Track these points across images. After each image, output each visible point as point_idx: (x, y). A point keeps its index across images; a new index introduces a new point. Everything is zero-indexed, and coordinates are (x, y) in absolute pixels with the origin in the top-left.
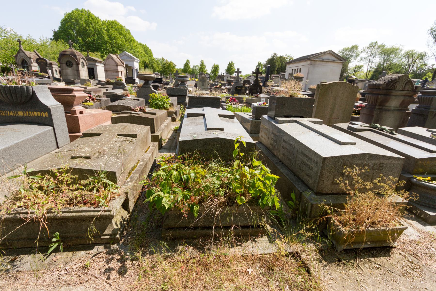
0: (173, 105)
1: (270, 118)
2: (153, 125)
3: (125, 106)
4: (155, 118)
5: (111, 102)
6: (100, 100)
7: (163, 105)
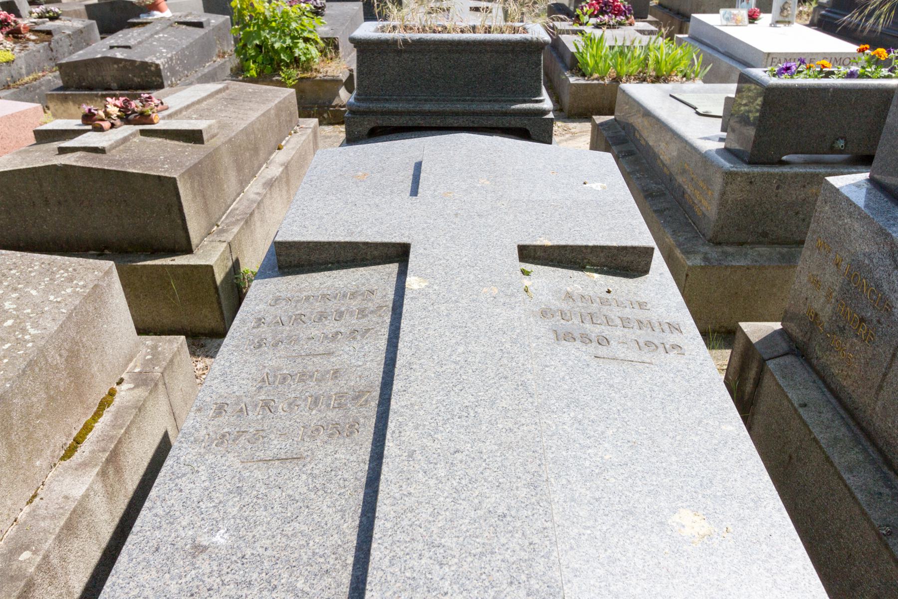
0: (336, 47)
1: (880, 195)
2: (175, 209)
3: (133, 62)
4: (194, 172)
5: (101, 33)
6: (49, 33)
7: (289, 49)
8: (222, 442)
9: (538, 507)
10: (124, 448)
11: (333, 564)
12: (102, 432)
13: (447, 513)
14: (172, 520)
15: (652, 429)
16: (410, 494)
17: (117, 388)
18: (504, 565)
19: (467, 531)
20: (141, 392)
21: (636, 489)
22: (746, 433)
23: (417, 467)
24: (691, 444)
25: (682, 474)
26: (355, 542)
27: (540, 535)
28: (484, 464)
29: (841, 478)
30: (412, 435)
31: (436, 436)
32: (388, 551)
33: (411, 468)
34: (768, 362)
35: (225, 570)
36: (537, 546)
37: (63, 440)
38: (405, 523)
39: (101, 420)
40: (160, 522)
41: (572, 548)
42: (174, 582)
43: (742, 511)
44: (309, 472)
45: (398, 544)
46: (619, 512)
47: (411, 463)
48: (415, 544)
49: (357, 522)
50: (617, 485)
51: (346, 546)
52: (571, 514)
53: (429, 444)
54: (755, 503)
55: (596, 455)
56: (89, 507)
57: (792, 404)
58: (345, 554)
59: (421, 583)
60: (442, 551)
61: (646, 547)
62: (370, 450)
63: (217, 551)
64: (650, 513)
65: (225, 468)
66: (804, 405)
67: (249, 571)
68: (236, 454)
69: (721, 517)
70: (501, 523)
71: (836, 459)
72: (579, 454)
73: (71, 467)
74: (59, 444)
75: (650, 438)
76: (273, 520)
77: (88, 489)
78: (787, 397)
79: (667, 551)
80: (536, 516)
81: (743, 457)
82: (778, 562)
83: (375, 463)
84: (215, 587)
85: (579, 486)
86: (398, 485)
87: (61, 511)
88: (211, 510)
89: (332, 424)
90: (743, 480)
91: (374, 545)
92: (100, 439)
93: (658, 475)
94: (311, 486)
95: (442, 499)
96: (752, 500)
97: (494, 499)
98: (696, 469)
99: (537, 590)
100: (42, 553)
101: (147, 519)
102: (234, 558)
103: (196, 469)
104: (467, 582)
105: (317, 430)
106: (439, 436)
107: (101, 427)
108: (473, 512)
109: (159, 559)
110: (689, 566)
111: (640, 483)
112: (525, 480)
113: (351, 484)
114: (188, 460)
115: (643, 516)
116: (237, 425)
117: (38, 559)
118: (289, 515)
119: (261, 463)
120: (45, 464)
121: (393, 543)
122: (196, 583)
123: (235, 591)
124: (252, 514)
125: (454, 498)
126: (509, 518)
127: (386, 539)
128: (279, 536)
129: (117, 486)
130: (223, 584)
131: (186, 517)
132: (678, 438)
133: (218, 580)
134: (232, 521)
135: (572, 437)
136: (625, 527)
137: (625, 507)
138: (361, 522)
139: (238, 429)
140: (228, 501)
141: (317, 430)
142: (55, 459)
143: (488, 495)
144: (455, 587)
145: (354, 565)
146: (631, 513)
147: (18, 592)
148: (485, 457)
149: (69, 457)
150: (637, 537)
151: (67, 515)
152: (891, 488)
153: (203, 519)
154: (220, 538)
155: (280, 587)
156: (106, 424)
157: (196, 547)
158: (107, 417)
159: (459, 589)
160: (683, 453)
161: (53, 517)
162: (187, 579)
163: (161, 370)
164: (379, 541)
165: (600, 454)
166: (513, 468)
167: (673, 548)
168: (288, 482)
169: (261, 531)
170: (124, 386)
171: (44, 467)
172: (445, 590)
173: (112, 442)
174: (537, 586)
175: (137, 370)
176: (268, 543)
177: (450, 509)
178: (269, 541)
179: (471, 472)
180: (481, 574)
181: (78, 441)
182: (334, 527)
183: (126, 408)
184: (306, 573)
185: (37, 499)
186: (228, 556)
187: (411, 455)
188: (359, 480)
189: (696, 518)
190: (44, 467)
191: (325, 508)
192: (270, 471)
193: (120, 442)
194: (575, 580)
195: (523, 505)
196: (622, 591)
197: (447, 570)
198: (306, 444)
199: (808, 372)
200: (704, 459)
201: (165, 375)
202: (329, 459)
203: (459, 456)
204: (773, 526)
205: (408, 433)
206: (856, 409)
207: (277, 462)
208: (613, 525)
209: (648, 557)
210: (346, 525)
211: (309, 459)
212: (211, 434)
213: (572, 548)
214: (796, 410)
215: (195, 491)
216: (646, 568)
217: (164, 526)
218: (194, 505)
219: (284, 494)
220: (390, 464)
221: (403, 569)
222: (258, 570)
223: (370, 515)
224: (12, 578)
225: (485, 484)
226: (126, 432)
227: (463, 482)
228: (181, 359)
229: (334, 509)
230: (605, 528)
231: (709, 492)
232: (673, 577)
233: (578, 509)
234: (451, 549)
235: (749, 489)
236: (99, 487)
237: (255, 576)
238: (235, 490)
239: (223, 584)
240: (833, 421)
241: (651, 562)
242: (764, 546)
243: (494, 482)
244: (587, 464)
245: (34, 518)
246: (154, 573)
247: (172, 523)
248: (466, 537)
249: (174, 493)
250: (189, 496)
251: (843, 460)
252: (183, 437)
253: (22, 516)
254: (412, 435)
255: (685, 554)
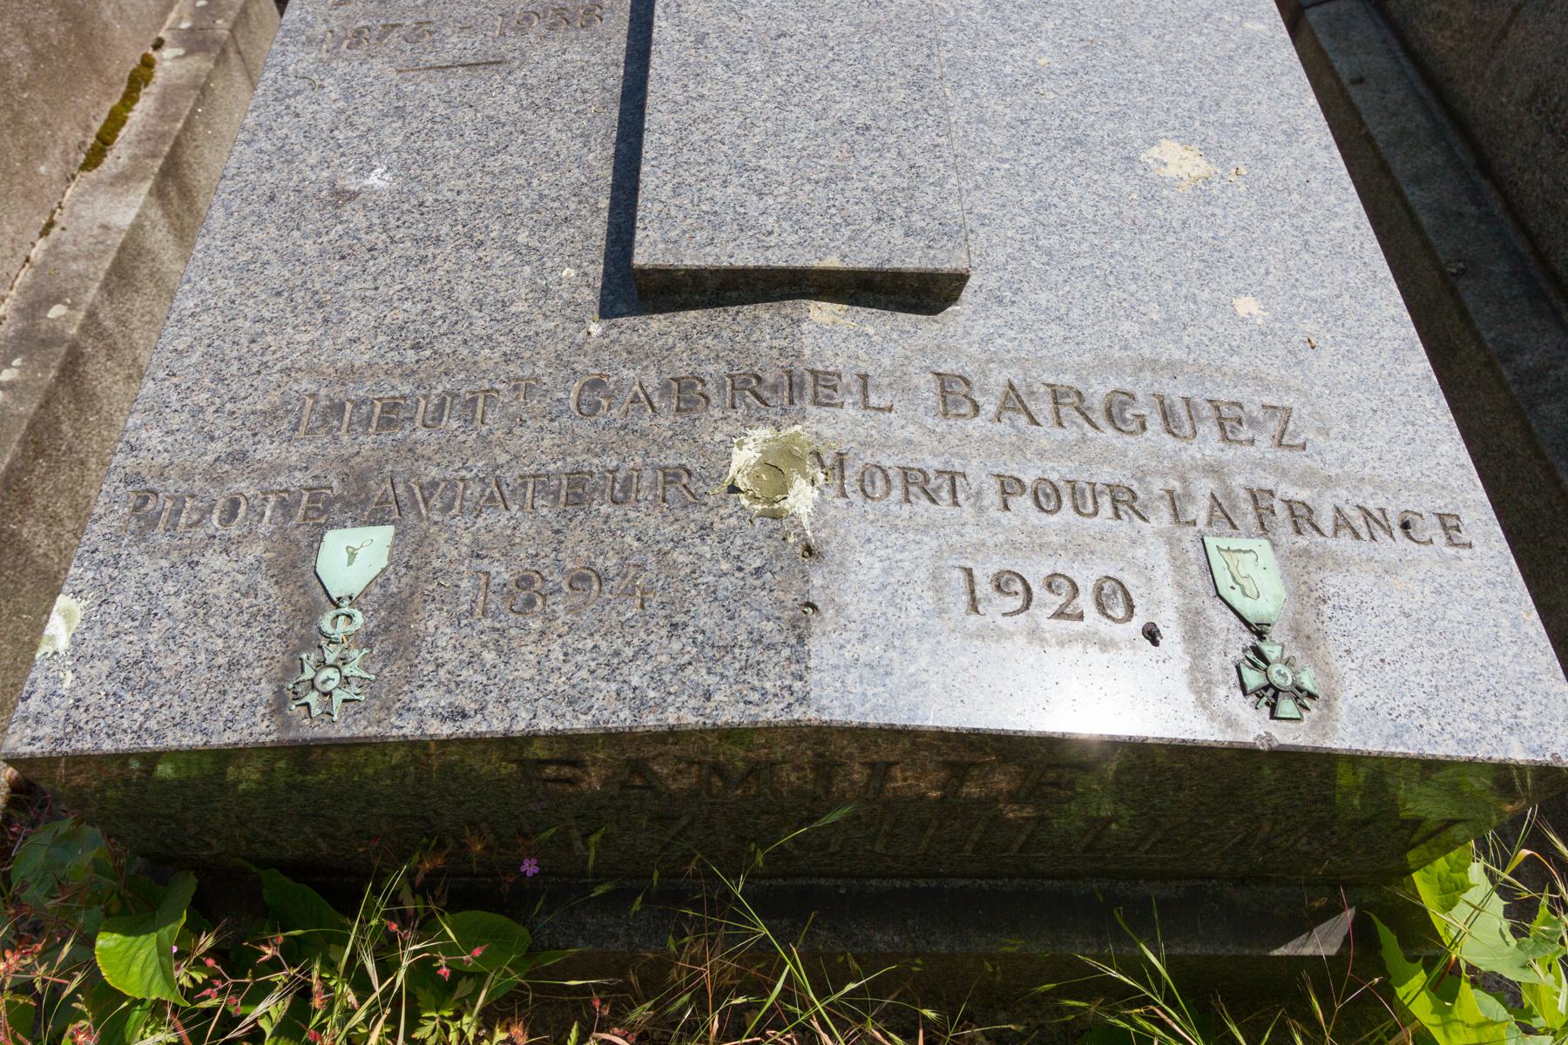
8: (359, 43)
9: (926, 116)
10: (188, 155)
11: (576, 210)
12: (144, 127)
13: (769, 124)
14: (289, 158)
15: (1124, 22)
16: (702, 96)
17: (155, 55)
18: (865, 195)
19: (804, 149)
20: (200, 64)
21: (1090, 109)
22: (1286, 35)
23: (712, 57)
24: (1189, 48)
25: (1170, 91)
26: (610, 178)
27: (928, 155)
28: (830, 54)
29: (1399, 194)
30: (700, 10)
31: (743, 12)
32: (669, 177)
33: (702, 59)
34: (1308, 12)
35: (393, 223)
36: (922, 170)
37: (75, 135)
38: (696, 137)
39: (138, 107)
40: (269, 161)
41: (977, 187)
42: (311, 241)
43: (1264, 146)
44: (519, 82)
45: (686, 167)
46: (1059, 141)
47: (702, 52)
48: (715, 167)
49: (612, 151)
50: (1057, 102)
51: (595, 185)
52: (978, 140)
53: (731, 24)
54: (1288, 136)
55: (1023, 57)
56: (148, 245)
57: (1338, 81)
58: (595, 195)
59: (728, 219)
60: (761, 176)
61: (1101, 191)
62: (625, 45)
63: (374, 197)
64: (1112, 144)
65: (369, 80)
66: (1359, 81)
67: (434, 224)
68: (386, 59)
69: (1229, 154)
70: (862, 138)
71: (1397, 164)
72: (993, 54)
73: (101, 182)
74: (72, 142)
75: (1119, 36)
76: (466, 153)
77: (138, 216)
78: (1331, 68)
79: (1135, 196)
80: (921, 128)
81: (1277, 69)
82: (1314, 217)
83: (635, 66)
84: (380, 245)
85: (993, 102)
86: (680, 84)
87: (101, 247)
88: (356, 141)
89: (554, 10)
90: (1273, 104)
91: (645, 168)
92: (143, 137)
93: (1129, 90)
94: (524, 102)
95: (758, 104)
96: (1284, 132)
97: (848, 105)
98: (1194, 85)
99: (922, 228)
100: (84, 307)
101: (246, 158)
102: (406, 207)
103: (318, 83)
104: (806, 218)
105: (527, 19)
106: (749, 12)
107: (139, 118)
108: (813, 123)
109: (276, 212)
110: (1169, 217)
111: (1098, 101)
112: (904, 77)
113: (596, 97)
114: (301, 71)
115: (1099, 148)
116: (381, 16)
117: (81, 316)
118: (492, 144)
119: (432, 72)
120: (56, 173)
121: (677, 165)
122: (347, 241)
123: (414, 250)
124: (426, 145)
125: (780, 103)
126: (874, 132)
127: (664, 159)
128: (479, 174)
129: (188, 219)
130: (393, 242)
131: (314, 153)
132: (1167, 38)
133: (384, 236)
134: (395, 156)
135: (984, 29)
136: (1068, 161)
137: (1069, 134)
138: (617, 150)
139: (383, 22)
140: (383, 127)
141: (527, 19)
142: (71, 167)
143: (838, 99)
144: (786, 225)
145: (612, 209)
146: (1079, 143)
147: (59, 361)
148: (831, 44)
149: (96, 166)
150: (1087, 175)
151: (113, 254)
152: (1479, 205)
153: (343, 155)
154: (377, 179)
155: (489, 243)
156: (148, 115)
157: (338, 193)
158: (145, 105)
159: (792, 226)
160: (1174, 60)
161: (89, 256)
162: (331, 237)
163: (228, 25)
164: (653, 163)
165: (1031, 56)
166: (881, 60)
167: (1145, 193)
168: (484, 97)
169: (446, 169)
170: (168, 53)
171: (55, 177)
172: (769, 228)
173: (164, 143)
174: (923, 224)
175: (185, 25)
176: (461, 184)
177: (773, 118)
178: (461, 182)
179: (807, 66)
180: (829, 207)
181: (105, 140)
182: (572, 159)
183: (178, 87)
184: (531, 223)
185: (55, 231)
186: (395, 205)
187: (701, 39)
188: (608, 91)
189: (1187, 154)
190: (55, 177)
191: (553, 132)
192: (449, 82)
193: (177, 143)
194: (981, 231)
195: (899, 113)
196: (1057, 247)
197: (771, 202)
198: (510, 41)
199: (1377, 25)
200: (1208, 71)
201: (238, 36)
202: (554, 62)
203: (785, 42)
204: (1313, 168)
205: (693, 7)
206: (1450, 80)
207: (460, 70)
208: (1048, 159)
209: (1104, 204)
210: (591, 156)
211: (517, 63)
212: (336, 29)
213: (977, 187)
214: (1343, 90)
215: (323, 115)
216: (1099, 219)
217: (278, 166)
218: (324, 136)
219: (479, 115)
220: (664, 53)
221: (696, 200)
222: (449, 221)
223: (632, 140)
224: (46, 343)
225: (833, 82)
226: (186, 128)
227: (795, 80)
228: (261, 9)
229: (569, 134)
230: (1033, 162)
231: (1212, 118)
232: (1142, 232)
233: (989, 134)
234: (777, 174)
235: (1280, 116)
236: (155, 213)
237: (445, 229)
238: (392, 112)
239: (393, 242)
240: (1404, 104)
241: (1107, 211)
242: (1295, 196)
243: (849, 79)
244: (1008, 69)
245: (57, 256)
246: (273, 230)
247: (291, 162)
248: (802, 157)
249: (286, 119)
250: (312, 122)
251: (1409, 166)
252: (285, 36)
253: (36, 254)
254: (700, 10)
255: (1164, 201)
